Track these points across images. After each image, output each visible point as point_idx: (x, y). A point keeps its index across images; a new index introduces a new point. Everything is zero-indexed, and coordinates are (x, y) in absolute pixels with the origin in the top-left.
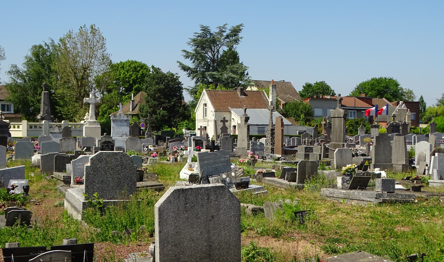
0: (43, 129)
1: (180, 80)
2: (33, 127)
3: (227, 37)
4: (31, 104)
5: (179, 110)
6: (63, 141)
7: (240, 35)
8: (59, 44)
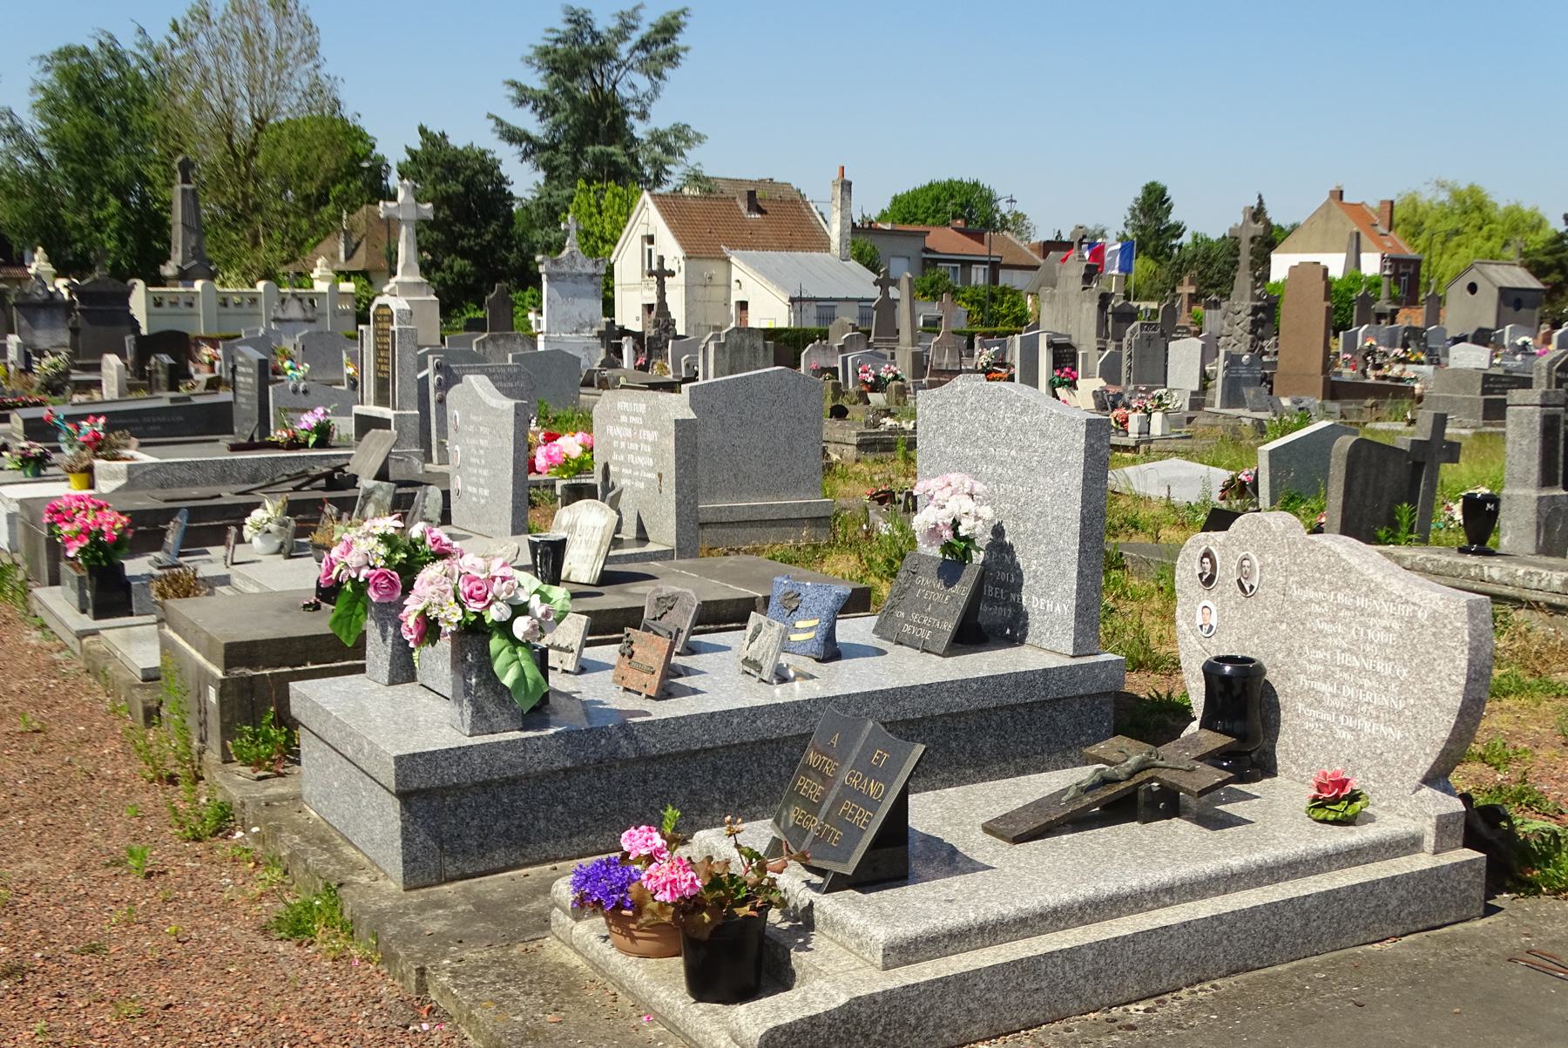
0: (200, 306)
1: (504, 171)
2: (166, 303)
3: (644, 45)
4: (75, 234)
5: (507, 259)
6: (490, 347)
7: (681, 40)
8: (170, 41)
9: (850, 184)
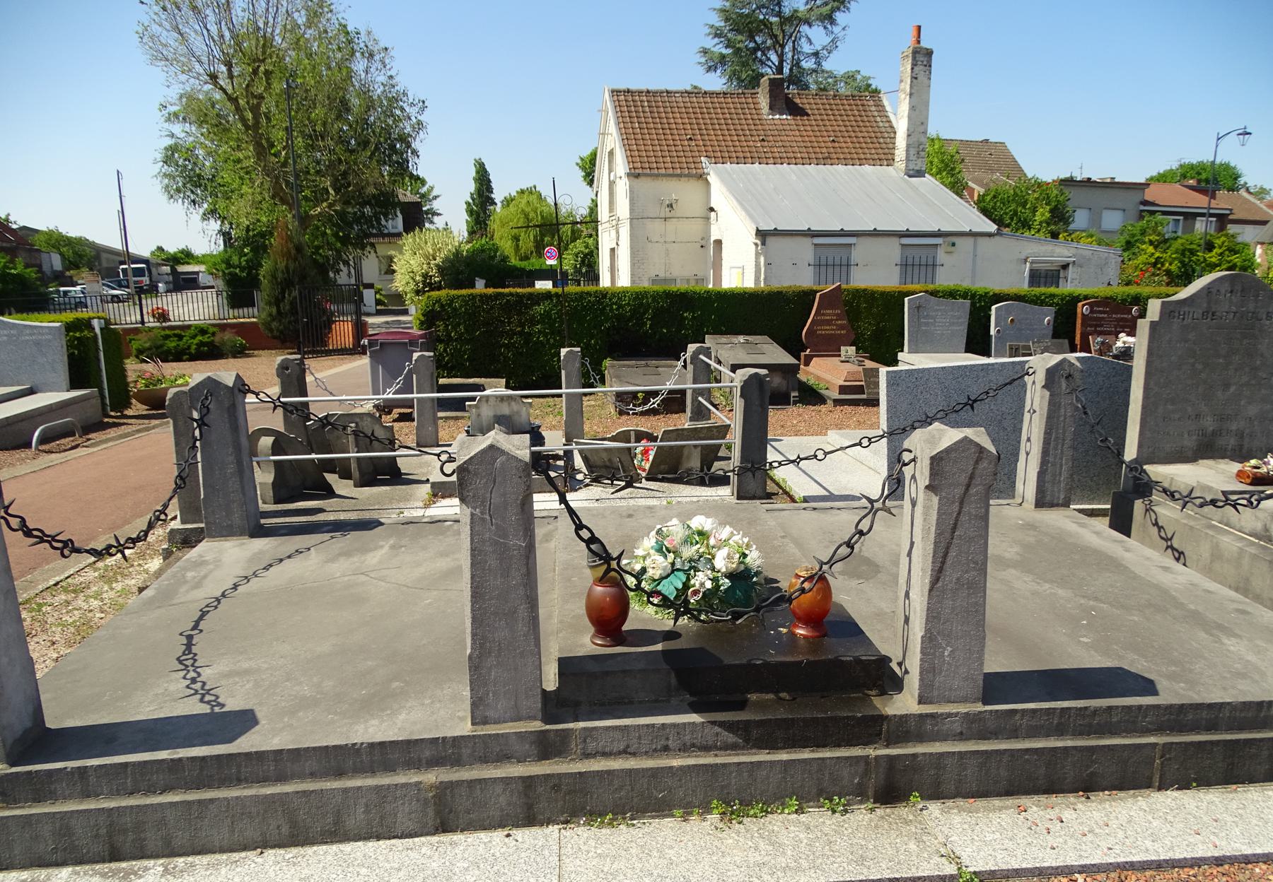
9: (929, 53)
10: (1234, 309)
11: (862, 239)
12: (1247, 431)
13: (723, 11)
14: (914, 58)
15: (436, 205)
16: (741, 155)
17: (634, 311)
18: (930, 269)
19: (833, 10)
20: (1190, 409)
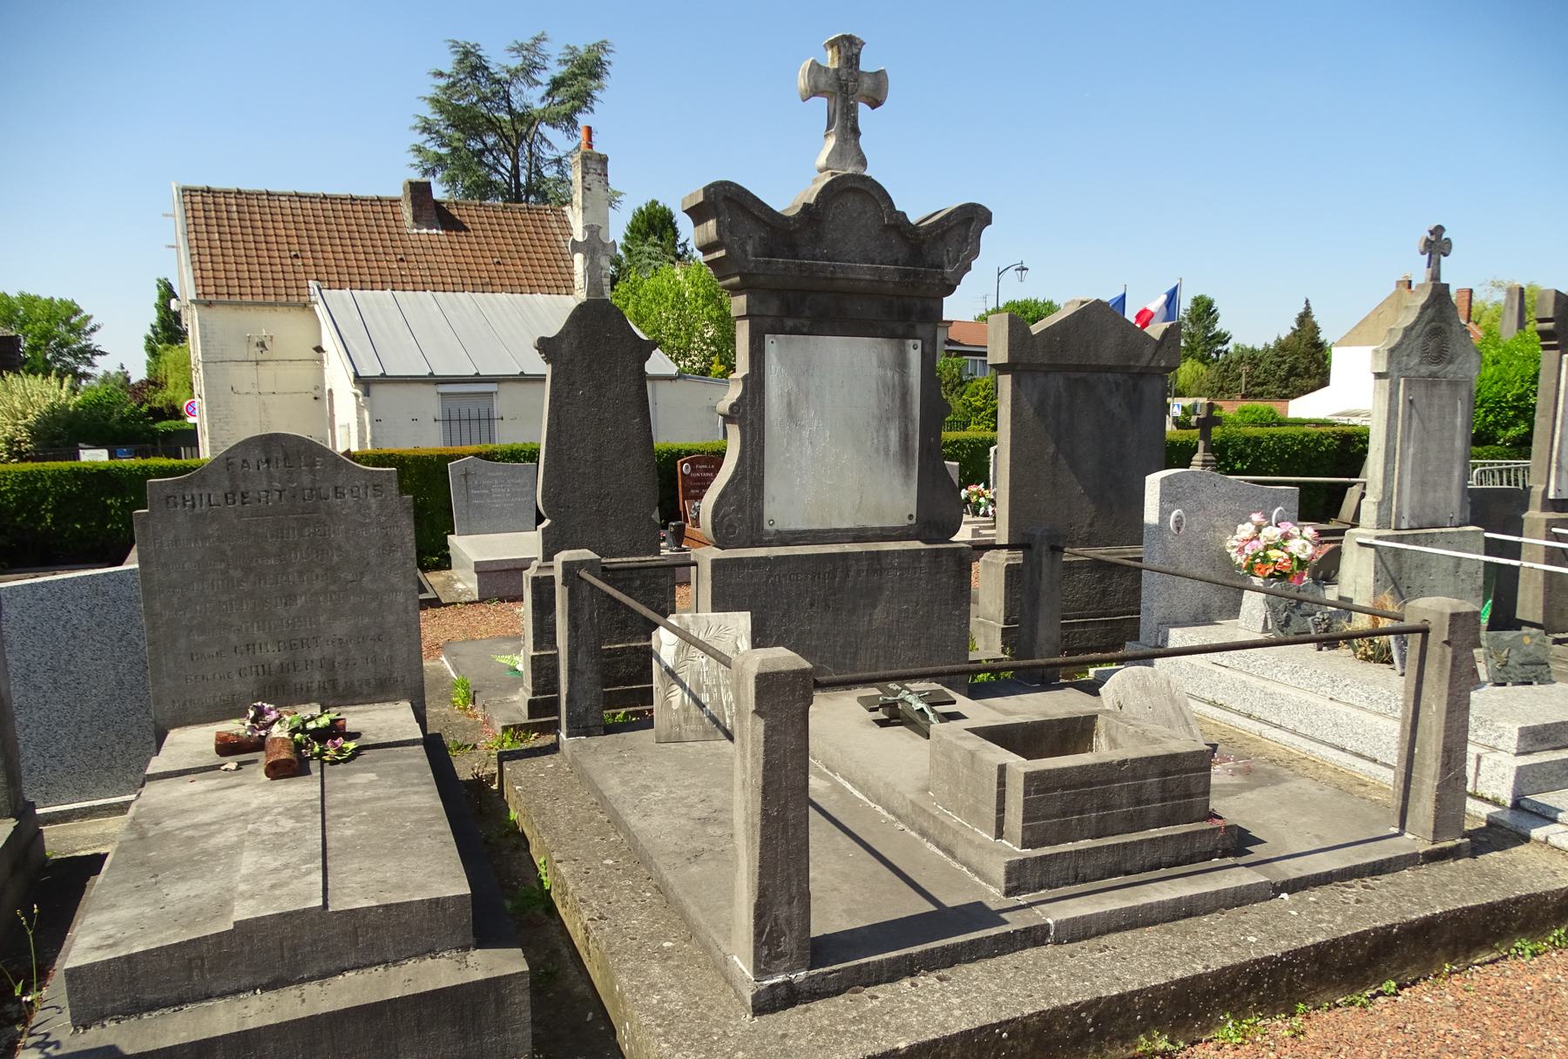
9: (603, 160)
10: (277, 485)
11: (505, 387)
12: (339, 659)
13: (435, 101)
14: (584, 165)
15: (96, 340)
16: (368, 278)
17: (23, 501)
18: (485, 424)
19: (577, 110)
20: (234, 638)
